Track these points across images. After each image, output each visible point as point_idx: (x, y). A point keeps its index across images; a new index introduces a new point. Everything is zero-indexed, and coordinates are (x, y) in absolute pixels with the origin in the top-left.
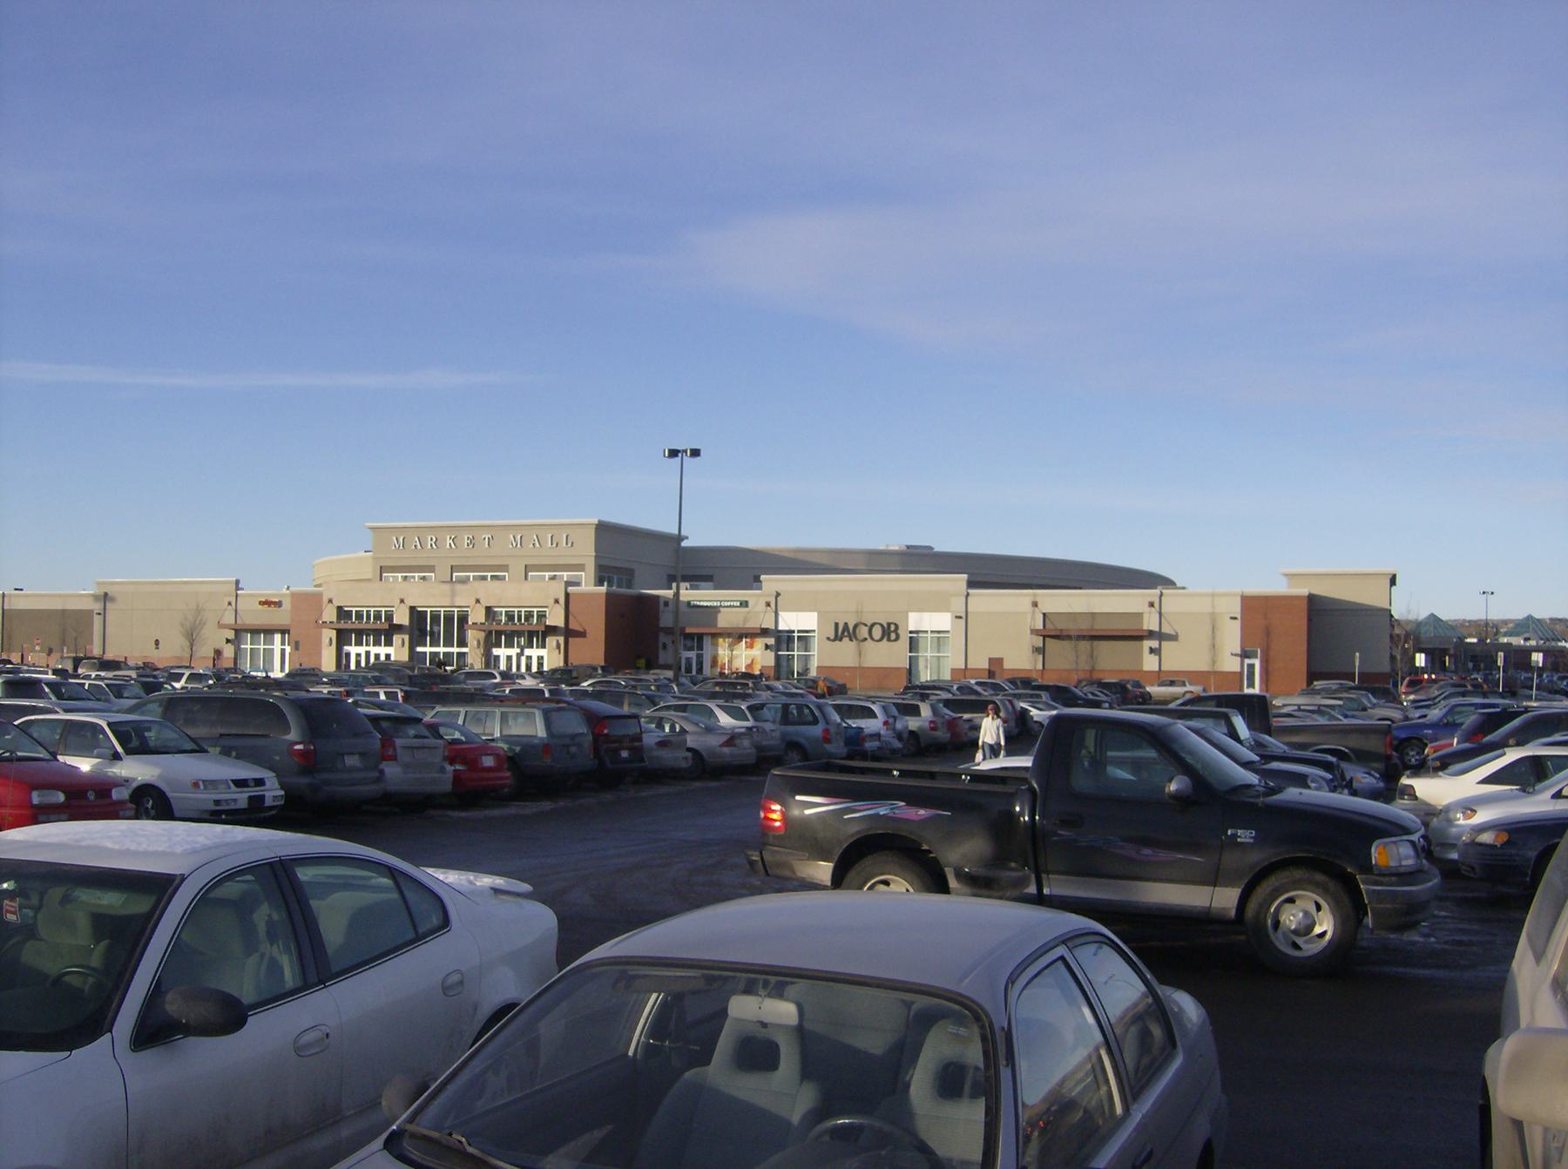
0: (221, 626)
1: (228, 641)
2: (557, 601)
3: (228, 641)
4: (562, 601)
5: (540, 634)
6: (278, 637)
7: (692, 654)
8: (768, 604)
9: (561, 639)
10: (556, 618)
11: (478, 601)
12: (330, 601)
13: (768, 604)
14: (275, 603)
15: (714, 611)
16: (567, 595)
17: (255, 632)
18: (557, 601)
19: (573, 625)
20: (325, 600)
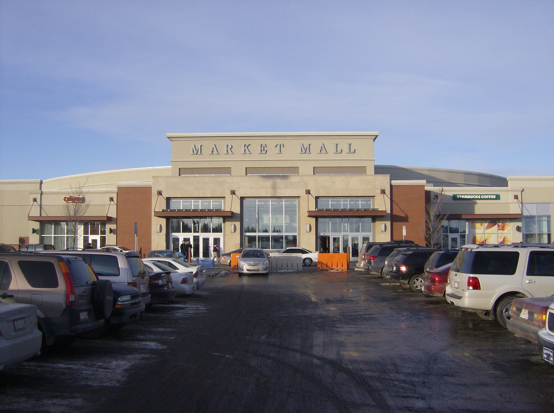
0: (31, 218)
1: (34, 231)
2: (383, 192)
3: (34, 231)
4: (388, 191)
5: (376, 216)
6: (81, 229)
7: (98, 237)
8: (35, 200)
9: (388, 223)
10: (382, 204)
11: (308, 192)
12: (160, 193)
13: (35, 200)
14: (78, 199)
15: (471, 202)
16: (391, 186)
17: (56, 222)
18: (383, 192)
19: (396, 212)
20: (154, 192)
